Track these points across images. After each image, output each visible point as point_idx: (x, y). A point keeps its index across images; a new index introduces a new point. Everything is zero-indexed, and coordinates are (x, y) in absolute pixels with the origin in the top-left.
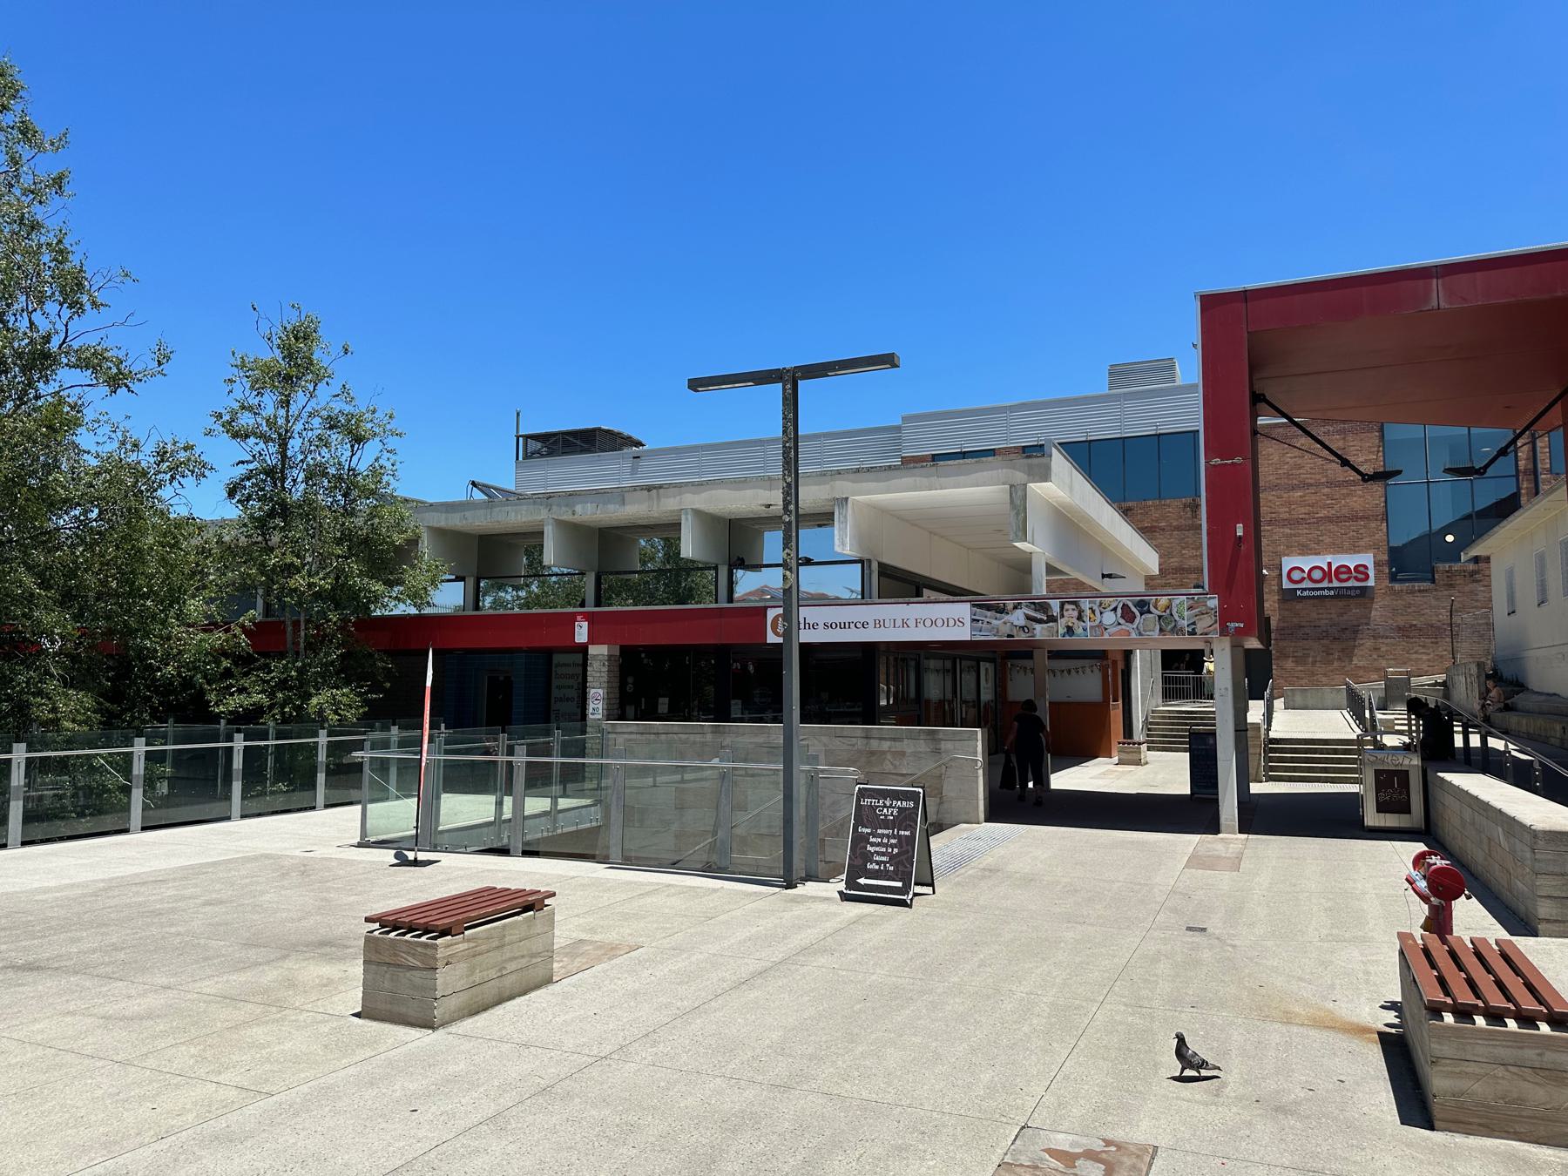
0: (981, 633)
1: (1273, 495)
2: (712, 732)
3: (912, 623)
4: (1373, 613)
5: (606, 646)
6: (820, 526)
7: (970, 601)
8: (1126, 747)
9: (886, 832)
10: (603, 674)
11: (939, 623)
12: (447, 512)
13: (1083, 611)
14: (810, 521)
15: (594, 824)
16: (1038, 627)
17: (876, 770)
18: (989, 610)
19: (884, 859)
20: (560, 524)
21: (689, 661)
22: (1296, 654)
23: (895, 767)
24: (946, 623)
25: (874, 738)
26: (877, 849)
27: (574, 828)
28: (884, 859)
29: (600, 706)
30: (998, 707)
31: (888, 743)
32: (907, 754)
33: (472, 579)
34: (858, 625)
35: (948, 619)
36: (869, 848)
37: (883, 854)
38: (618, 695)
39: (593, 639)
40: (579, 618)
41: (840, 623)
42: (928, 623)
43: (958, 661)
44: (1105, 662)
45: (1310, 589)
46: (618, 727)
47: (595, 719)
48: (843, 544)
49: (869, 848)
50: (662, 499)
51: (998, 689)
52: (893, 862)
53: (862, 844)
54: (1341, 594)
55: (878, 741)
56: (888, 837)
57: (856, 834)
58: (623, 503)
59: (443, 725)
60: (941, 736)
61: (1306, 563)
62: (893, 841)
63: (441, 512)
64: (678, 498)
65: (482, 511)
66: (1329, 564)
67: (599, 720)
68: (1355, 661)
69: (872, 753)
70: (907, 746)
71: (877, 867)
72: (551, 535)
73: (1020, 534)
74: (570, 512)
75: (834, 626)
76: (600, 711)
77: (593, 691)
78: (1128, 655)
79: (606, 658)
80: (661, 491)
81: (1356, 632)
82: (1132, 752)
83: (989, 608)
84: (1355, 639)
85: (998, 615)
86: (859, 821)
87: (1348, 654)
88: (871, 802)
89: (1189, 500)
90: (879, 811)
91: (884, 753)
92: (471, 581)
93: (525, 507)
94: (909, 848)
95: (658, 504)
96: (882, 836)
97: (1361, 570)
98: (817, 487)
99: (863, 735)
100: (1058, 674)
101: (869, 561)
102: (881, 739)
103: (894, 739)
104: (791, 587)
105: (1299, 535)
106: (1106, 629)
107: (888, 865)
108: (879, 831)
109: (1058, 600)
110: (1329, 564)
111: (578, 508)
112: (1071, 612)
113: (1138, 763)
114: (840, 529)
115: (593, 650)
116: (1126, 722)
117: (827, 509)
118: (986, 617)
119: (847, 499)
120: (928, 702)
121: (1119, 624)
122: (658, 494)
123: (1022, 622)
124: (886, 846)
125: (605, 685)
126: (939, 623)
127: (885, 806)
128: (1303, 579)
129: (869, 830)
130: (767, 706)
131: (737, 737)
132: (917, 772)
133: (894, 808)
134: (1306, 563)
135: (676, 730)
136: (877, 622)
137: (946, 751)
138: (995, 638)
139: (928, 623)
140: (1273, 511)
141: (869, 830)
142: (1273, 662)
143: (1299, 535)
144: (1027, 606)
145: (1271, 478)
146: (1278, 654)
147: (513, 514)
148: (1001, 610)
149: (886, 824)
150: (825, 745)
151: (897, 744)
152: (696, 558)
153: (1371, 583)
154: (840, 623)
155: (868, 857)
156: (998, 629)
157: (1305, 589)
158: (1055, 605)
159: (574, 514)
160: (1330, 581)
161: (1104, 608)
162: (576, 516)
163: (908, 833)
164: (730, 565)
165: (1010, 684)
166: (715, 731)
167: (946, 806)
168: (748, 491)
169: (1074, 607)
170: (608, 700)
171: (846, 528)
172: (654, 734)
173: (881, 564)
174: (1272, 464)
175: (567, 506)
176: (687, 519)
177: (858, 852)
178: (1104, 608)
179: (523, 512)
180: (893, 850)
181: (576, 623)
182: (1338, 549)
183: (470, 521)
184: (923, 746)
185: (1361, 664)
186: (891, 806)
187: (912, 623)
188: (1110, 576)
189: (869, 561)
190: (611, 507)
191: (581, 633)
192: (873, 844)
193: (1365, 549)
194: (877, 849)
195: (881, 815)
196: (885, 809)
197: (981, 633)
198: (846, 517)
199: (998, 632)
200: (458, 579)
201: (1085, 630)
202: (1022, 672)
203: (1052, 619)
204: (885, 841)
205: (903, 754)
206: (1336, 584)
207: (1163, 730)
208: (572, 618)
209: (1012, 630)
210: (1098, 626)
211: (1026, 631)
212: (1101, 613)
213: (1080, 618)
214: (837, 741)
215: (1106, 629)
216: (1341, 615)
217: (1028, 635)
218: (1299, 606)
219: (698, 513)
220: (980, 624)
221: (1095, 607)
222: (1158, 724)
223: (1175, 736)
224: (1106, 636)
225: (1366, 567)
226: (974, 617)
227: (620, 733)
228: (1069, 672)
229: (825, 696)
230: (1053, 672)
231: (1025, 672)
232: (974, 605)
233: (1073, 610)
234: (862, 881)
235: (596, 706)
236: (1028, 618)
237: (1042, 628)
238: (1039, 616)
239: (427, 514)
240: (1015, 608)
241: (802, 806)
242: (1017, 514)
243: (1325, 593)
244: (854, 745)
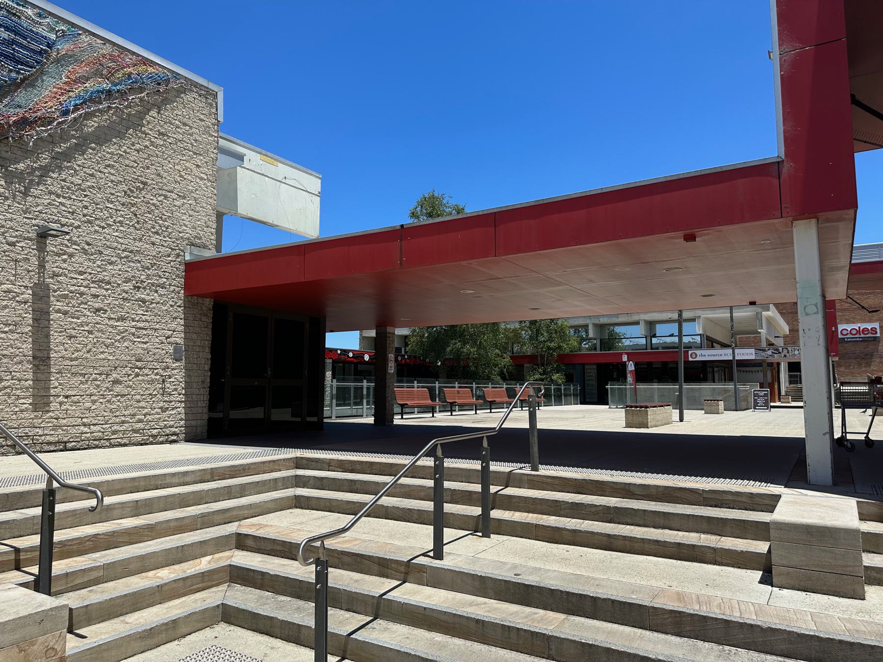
4: (880, 347)
16: (776, 355)
39: (629, 360)
45: (851, 338)
54: (865, 340)
61: (849, 327)
66: (859, 328)
68: (872, 368)
78: (779, 364)
81: (872, 356)
84: (871, 359)
86: (754, 396)
87: (868, 365)
97: (874, 330)
100: (754, 372)
105: (846, 315)
110: (859, 328)
111: (601, 319)
116: (163, 636)
123: (771, 354)
128: (848, 334)
130: (674, 379)
134: (849, 327)
143: (846, 315)
148: (764, 351)
149: (761, 396)
153: (878, 335)
157: (849, 338)
160: (860, 334)
182: (864, 321)
185: (875, 369)
188: (778, 337)
190: (614, 319)
193: (875, 321)
203: (780, 353)
206: (862, 336)
208: (622, 354)
213: (788, 352)
216: (866, 348)
218: (846, 345)
225: (876, 328)
228: (758, 371)
230: (755, 372)
236: (772, 352)
238: (775, 352)
243: (858, 339)
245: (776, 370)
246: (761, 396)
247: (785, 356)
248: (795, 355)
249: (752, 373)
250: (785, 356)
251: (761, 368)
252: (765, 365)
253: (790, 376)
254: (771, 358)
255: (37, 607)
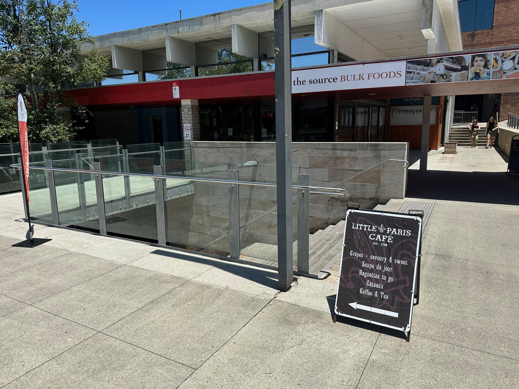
0: (412, 81)
1: (512, 28)
2: (246, 147)
3: (365, 77)
5: (190, 100)
6: (306, 35)
7: (406, 60)
8: (449, 146)
9: (380, 259)
10: (189, 116)
11: (384, 75)
12: (122, 37)
13: (489, 61)
14: (301, 32)
15: (190, 193)
16: (454, 74)
17: (339, 168)
18: (419, 65)
19: (377, 286)
20: (173, 39)
21: (241, 109)
22: (512, 102)
23: (351, 166)
24: (389, 75)
25: (338, 149)
26: (370, 275)
27: (178, 196)
28: (377, 286)
29: (190, 133)
30: (386, 129)
31: (347, 152)
32: (359, 159)
33: (141, 72)
34: (331, 80)
35: (390, 73)
36: (361, 273)
37: (377, 281)
38: (199, 127)
39: (183, 95)
40: (174, 84)
41: (319, 80)
42: (376, 76)
43: (371, 107)
44: (439, 106)
46: (198, 144)
47: (188, 140)
48: (319, 38)
49: (361, 273)
50: (221, 21)
51: (386, 120)
52: (388, 291)
53: (354, 269)
55: (341, 151)
56: (382, 264)
57: (347, 258)
58: (202, 24)
59: (118, 143)
60: (381, 147)
62: (387, 269)
63: (119, 37)
64: (229, 19)
65: (137, 35)
67: (190, 140)
69: (337, 158)
70: (359, 154)
71: (370, 294)
72: (169, 45)
73: (427, 23)
74: (177, 32)
75: (315, 81)
76: (190, 136)
77: (185, 125)
79: (190, 107)
80: (221, 15)
82: (452, 148)
83: (419, 63)
85: (425, 68)
88: (363, 227)
89: (471, 32)
90: (372, 237)
91: (344, 158)
92: (141, 73)
93: (155, 31)
94: (407, 278)
95: (219, 24)
96: (376, 262)
98: (304, 5)
99: (332, 148)
101: (333, 51)
102: (343, 150)
103: (351, 150)
104: (282, 8)
106: (505, 73)
107: (382, 293)
108: (373, 257)
109: (471, 55)
111: (180, 29)
112: (480, 62)
113: (454, 152)
114: (318, 30)
115: (184, 102)
117: (308, 22)
118: (417, 70)
119: (322, 10)
120: (357, 127)
121: (516, 69)
122: (219, 17)
124: (380, 273)
125: (191, 122)
126: (384, 75)
127: (378, 232)
129: (361, 255)
131: (260, 149)
132: (364, 169)
133: (388, 235)
135: (227, 145)
136: (343, 77)
137: (384, 157)
138: (422, 84)
139: (376, 76)
140: (511, 35)
141: (361, 255)
142: (501, 106)
144: (447, 60)
145: (512, 19)
146: (504, 102)
147: (151, 35)
149: (379, 250)
150: (309, 154)
151: (353, 153)
152: (240, 54)
154: (319, 80)
155: (361, 282)
156: (424, 77)
158: (468, 58)
159: (178, 33)
161: (505, 58)
162: (180, 34)
163: (404, 263)
164: (259, 58)
165: (392, 118)
166: (248, 146)
167: (381, 188)
168: (266, 11)
169: (482, 58)
170: (194, 129)
171: (321, 29)
172: (217, 148)
173: (339, 54)
174: (513, 12)
175: (175, 28)
176: (234, 31)
177: (350, 276)
178: (505, 58)
179: (155, 34)
180: (387, 279)
181: (173, 87)
183: (132, 41)
184: (369, 154)
186: (385, 233)
187: (365, 77)
189: (333, 51)
190: (196, 27)
191: (176, 93)
192: (365, 270)
194: (370, 275)
195: (374, 241)
196: (379, 236)
197: (412, 81)
198: (321, 22)
199: (424, 79)
200: (136, 73)
201: (488, 74)
202: (398, 112)
203: (465, 68)
204: (379, 267)
205: (356, 158)
207: (456, 136)
209: (434, 78)
210: (499, 71)
211: (445, 77)
212: (502, 62)
213: (486, 66)
214: (316, 152)
215: (505, 73)
217: (445, 80)
219: (241, 28)
220: (412, 74)
221: (499, 58)
222: (454, 134)
223: (462, 139)
224: (504, 78)
226: (408, 70)
227: (199, 147)
228: (413, 111)
229: (307, 126)
230: (413, 111)
231: (400, 112)
232: (409, 62)
233: (481, 60)
234: (354, 305)
235: (188, 133)
237: (457, 75)
238: (455, 66)
239: (113, 39)
240: (438, 62)
241: (295, 220)
242: (427, 11)
244: (326, 154)
245: (443, 108)
246: (379, 250)
247: (477, 75)
248: (502, 72)
249: (400, 112)
250: (477, 75)
251: (421, 107)
252: (428, 101)
253: (455, 115)
254: (442, 82)
255: (17, 253)
